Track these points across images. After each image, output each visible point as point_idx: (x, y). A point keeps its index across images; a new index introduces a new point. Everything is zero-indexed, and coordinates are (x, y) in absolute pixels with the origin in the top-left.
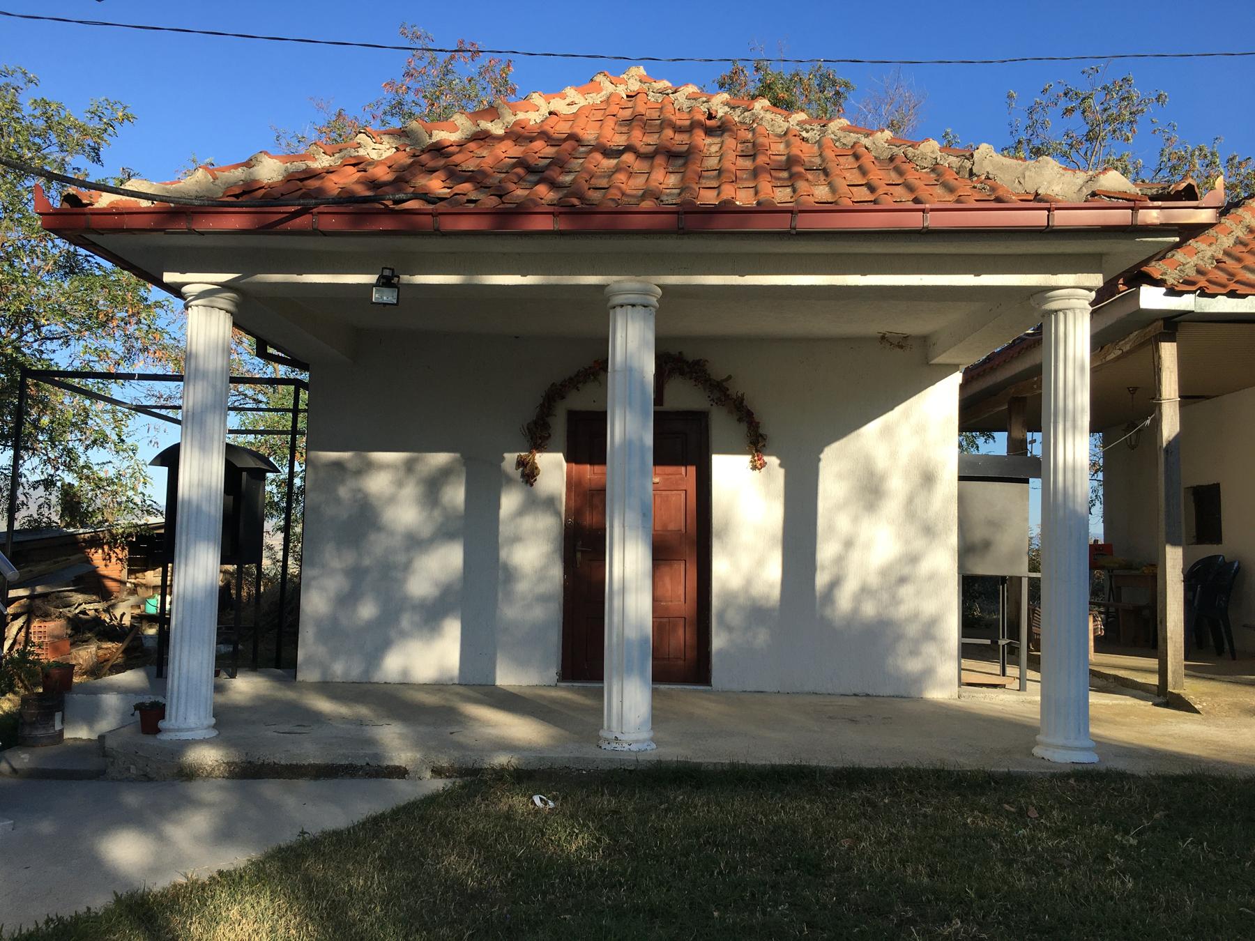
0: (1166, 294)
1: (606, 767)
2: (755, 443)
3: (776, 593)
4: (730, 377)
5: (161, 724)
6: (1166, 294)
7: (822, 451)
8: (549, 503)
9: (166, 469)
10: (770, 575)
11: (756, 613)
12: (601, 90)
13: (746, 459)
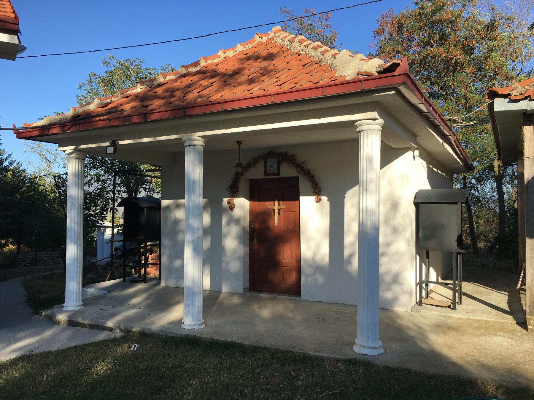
0: (508, 102)
1: (171, 335)
2: (317, 190)
3: (327, 259)
4: (304, 161)
5: (64, 305)
6: (508, 102)
7: (345, 193)
8: (237, 221)
9: (123, 207)
10: (325, 249)
11: (318, 268)
12: (255, 41)
13: (313, 198)
